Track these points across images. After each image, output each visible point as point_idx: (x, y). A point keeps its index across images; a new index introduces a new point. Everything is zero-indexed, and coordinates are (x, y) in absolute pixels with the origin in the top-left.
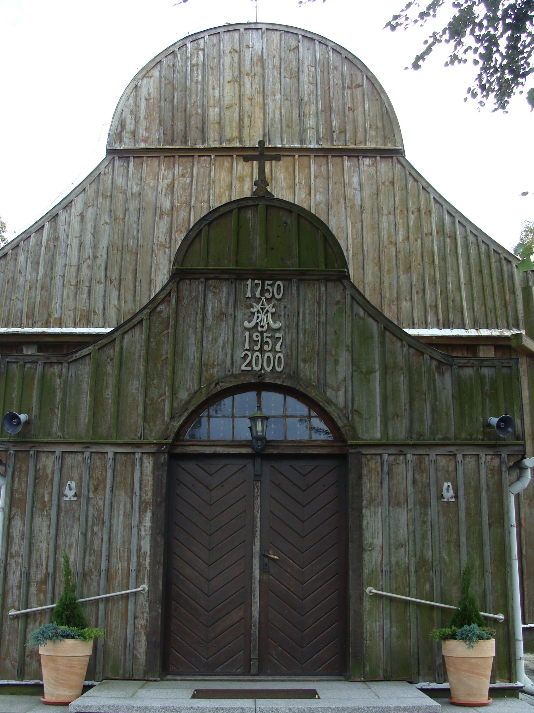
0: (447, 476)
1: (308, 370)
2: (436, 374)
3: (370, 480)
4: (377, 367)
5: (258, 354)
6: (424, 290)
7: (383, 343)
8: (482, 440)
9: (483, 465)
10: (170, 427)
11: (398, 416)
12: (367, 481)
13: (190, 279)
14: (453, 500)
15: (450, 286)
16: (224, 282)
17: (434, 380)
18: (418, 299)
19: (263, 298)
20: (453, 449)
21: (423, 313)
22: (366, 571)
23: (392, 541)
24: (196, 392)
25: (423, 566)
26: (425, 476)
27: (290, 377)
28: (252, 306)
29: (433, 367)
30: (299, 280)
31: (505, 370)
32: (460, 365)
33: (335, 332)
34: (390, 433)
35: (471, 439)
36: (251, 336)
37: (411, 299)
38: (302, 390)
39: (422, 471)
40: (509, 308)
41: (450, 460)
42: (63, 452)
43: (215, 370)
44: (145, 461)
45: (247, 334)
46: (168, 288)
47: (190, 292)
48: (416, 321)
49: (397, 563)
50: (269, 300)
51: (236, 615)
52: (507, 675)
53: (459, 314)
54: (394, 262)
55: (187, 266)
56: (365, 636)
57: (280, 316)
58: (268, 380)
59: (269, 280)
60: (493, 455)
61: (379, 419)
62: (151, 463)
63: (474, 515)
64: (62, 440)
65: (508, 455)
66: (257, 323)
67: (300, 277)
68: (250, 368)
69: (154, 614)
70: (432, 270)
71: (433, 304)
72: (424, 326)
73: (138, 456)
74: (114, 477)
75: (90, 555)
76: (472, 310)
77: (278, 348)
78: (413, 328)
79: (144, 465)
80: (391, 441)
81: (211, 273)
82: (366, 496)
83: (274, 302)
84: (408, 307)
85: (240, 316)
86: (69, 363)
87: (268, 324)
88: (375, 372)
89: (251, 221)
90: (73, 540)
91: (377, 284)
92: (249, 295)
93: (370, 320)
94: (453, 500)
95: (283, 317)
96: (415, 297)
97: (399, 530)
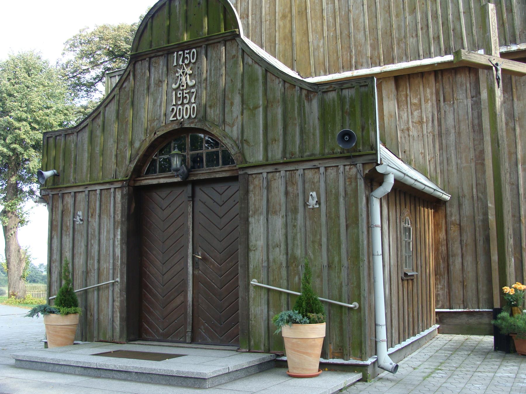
0: (313, 187)
1: (213, 113)
2: (305, 101)
3: (254, 194)
4: (261, 103)
5: (180, 107)
6: (427, 26)
7: (265, 83)
8: (341, 153)
9: (341, 174)
10: (129, 168)
11: (276, 140)
12: (253, 195)
13: (141, 60)
14: (318, 206)
15: (450, 17)
16: (160, 58)
17: (304, 106)
18: (422, 34)
19: (184, 64)
20: (316, 163)
21: (427, 45)
22: (251, 266)
23: (270, 243)
24: (143, 141)
25: (294, 262)
26: (295, 188)
27: (200, 121)
28: (177, 72)
29: (303, 95)
30: (207, 45)
31: (363, 89)
32: (324, 90)
33: (232, 80)
34: (270, 155)
35: (333, 153)
36: (176, 95)
37: (417, 35)
38: (207, 130)
39: (293, 184)
40: (507, 26)
41: (316, 172)
42: (75, 192)
43: (155, 123)
44: (117, 193)
45: (174, 92)
46: (128, 70)
47: (142, 69)
48: (421, 53)
49: (274, 261)
50: (187, 65)
51: (179, 300)
52: (359, 354)
53: (460, 41)
54: (402, 6)
55: (140, 51)
56: (250, 317)
57: (195, 75)
58: (186, 125)
59: (187, 50)
60: (351, 165)
61: (261, 145)
62: (120, 194)
63: (333, 219)
64: (75, 184)
65: (363, 164)
66: (180, 84)
67: (206, 43)
68: (175, 119)
69: (122, 298)
70: (434, 6)
71: (436, 35)
72: (429, 56)
73: (112, 190)
74: (100, 206)
75: (90, 260)
76: (471, 35)
77: (193, 100)
78: (419, 59)
79: (116, 196)
80: (270, 162)
81: (151, 53)
82: (252, 207)
83: (191, 65)
84: (414, 43)
85: (170, 80)
86: (78, 132)
87: (187, 83)
88: (259, 107)
89: (178, 8)
90: (82, 250)
91: (388, 28)
92: (175, 64)
93: (256, 66)
94: (318, 206)
95: (197, 76)
96: (420, 32)
97: (275, 233)
